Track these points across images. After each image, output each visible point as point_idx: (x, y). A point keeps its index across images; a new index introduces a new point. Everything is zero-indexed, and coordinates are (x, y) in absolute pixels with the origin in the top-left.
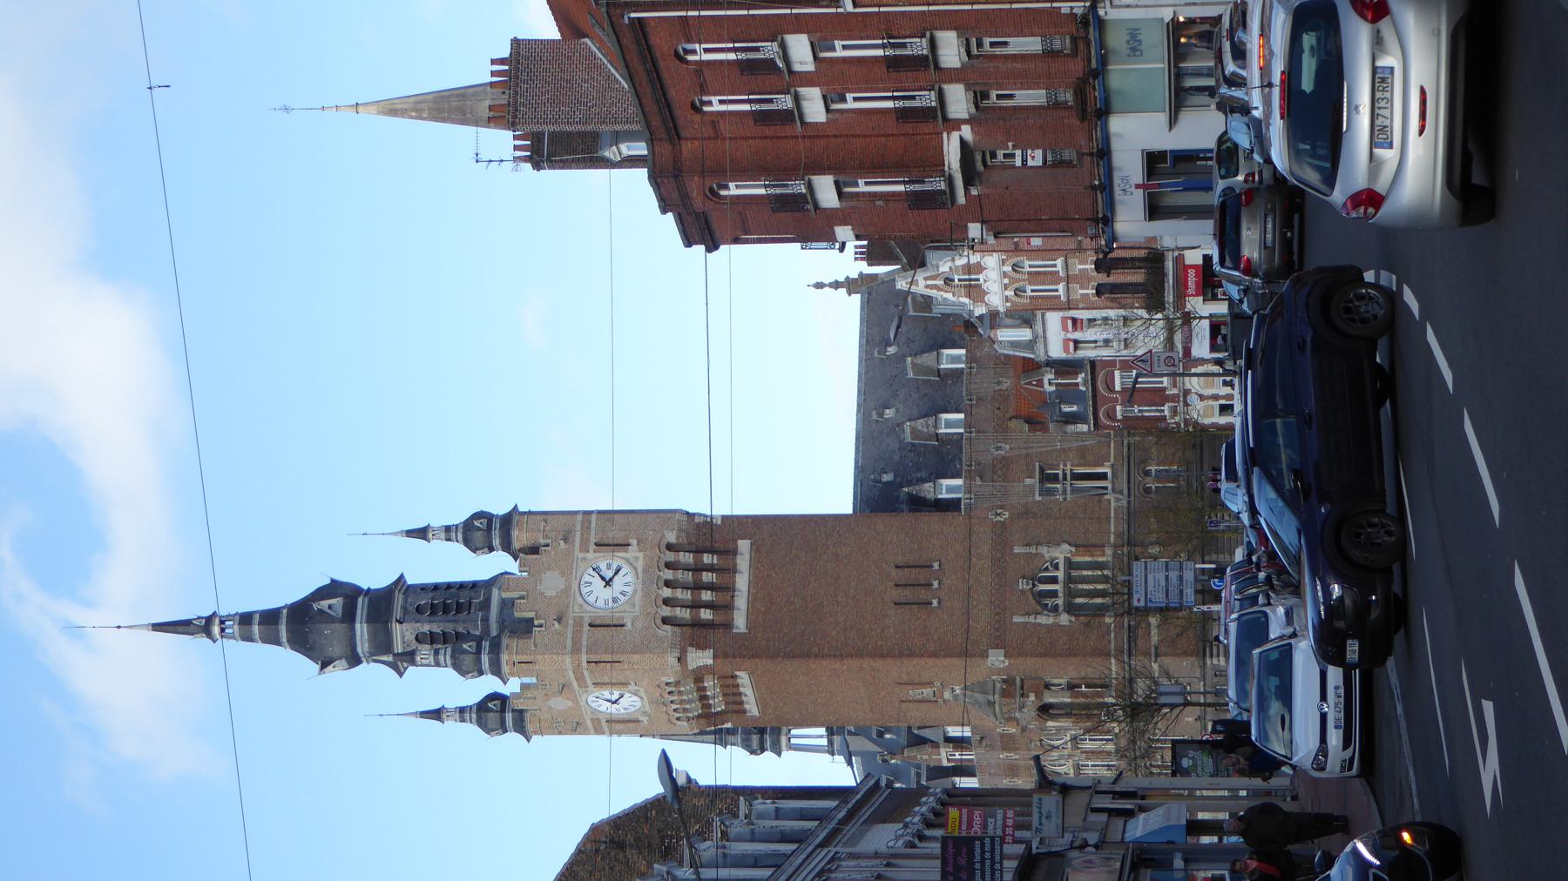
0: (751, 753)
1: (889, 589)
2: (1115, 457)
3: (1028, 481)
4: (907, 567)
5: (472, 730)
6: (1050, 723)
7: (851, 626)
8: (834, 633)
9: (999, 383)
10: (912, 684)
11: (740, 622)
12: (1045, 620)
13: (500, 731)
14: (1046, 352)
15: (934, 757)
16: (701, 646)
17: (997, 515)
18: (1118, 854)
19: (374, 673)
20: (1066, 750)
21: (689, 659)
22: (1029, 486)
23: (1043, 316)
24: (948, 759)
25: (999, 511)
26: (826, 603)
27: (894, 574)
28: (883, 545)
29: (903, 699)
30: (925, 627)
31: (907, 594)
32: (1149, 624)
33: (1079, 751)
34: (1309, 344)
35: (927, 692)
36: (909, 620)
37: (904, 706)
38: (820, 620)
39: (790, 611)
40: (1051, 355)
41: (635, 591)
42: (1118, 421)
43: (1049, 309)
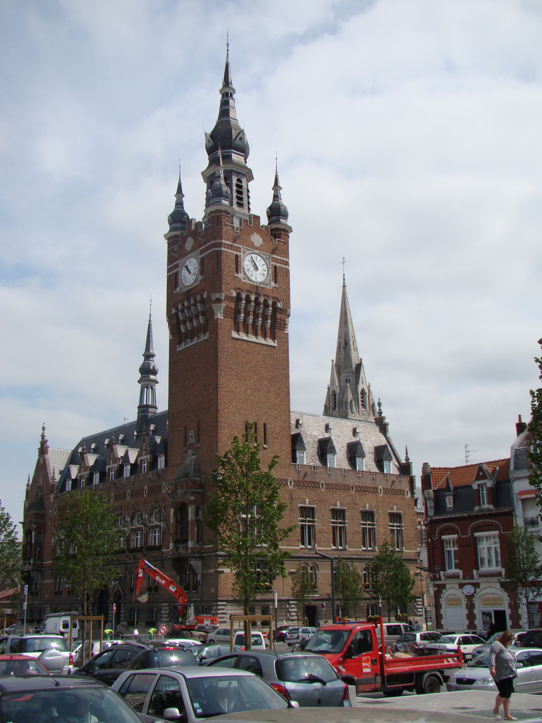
1: (254, 418)
3: (307, 501)
6: (172, 511)
7: (234, 395)
8: (231, 385)
13: (171, 221)
15: (144, 452)
17: (291, 482)
20: (148, 523)
22: (305, 501)
26: (246, 383)
27: (261, 422)
28: (275, 417)
33: (148, 530)
34: (86, 622)
38: (238, 379)
39: (242, 363)
42: (440, 537)
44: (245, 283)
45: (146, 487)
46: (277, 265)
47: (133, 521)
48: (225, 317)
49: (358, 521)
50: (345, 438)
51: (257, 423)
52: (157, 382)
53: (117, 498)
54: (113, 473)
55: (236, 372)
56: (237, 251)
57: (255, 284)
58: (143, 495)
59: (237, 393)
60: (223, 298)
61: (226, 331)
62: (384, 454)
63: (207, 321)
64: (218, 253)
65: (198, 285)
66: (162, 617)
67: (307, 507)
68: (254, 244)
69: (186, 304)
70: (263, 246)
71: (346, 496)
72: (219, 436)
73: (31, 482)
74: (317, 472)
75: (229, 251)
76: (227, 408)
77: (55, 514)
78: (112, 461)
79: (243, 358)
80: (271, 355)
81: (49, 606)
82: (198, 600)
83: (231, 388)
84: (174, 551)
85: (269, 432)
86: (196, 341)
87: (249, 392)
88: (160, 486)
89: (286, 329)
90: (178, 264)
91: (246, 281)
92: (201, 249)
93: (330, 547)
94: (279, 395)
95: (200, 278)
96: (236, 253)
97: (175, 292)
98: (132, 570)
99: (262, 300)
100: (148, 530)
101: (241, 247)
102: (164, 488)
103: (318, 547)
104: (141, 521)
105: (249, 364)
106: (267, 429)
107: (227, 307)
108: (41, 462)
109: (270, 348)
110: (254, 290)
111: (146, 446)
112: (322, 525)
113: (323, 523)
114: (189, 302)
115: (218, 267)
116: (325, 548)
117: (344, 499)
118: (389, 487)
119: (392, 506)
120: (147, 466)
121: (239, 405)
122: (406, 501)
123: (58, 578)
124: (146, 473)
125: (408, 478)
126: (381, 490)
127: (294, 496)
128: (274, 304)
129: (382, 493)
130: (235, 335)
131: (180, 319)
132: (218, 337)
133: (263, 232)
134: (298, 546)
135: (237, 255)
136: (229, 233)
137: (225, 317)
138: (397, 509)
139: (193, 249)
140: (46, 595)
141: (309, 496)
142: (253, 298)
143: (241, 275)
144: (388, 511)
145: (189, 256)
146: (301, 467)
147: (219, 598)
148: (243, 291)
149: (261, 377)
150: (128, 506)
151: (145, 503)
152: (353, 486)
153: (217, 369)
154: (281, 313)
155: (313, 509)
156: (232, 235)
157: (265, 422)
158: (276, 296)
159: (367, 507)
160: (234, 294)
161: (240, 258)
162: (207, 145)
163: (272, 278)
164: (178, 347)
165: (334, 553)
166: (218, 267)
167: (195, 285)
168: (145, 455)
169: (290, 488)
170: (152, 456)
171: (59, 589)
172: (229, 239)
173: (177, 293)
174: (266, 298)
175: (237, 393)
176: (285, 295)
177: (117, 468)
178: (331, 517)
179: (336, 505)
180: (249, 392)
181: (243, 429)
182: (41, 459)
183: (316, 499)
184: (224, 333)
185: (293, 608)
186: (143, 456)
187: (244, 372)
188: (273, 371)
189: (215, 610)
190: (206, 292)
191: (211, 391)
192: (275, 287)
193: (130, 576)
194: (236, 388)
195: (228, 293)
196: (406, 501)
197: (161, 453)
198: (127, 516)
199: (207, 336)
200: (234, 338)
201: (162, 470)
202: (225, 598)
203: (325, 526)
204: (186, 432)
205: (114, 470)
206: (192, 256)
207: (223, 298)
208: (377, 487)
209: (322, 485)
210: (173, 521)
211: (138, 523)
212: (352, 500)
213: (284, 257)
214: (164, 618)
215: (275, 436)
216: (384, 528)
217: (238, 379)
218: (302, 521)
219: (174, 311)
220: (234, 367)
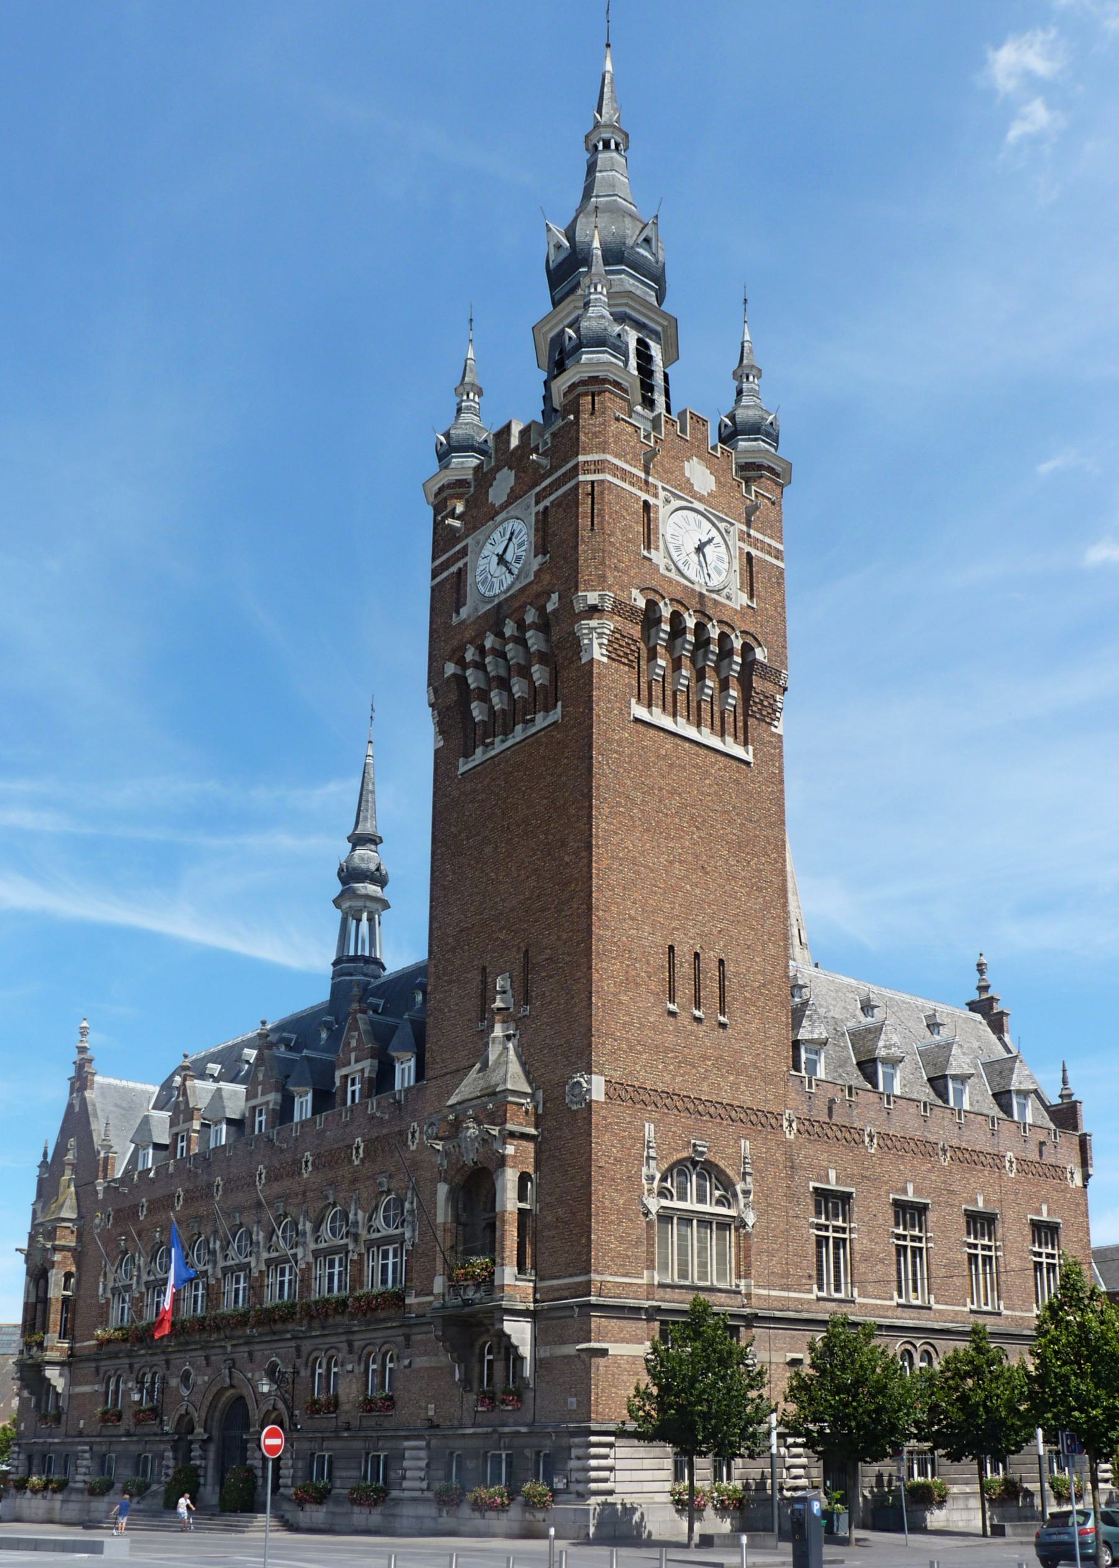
1: (691, 942)
2: (864, 1305)
6: (443, 1189)
15: (353, 1055)
18: (747, 407)
22: (827, 1175)
24: (346, 1076)
30: (637, 985)
31: (685, 969)
36: (648, 962)
37: (475, 976)
39: (661, 789)
44: (670, 581)
45: (359, 1139)
46: (754, 552)
47: (318, 1231)
48: (613, 659)
49: (957, 1236)
50: (909, 1034)
51: (701, 956)
52: (386, 905)
53: (274, 1176)
54: (263, 1118)
55: (642, 811)
56: (647, 492)
57: (697, 588)
58: (351, 1162)
59: (646, 867)
60: (608, 605)
61: (616, 696)
62: (1015, 1076)
64: (593, 487)
65: (531, 583)
66: (404, 1478)
67: (832, 1191)
68: (692, 485)
69: (489, 642)
70: (715, 497)
71: (929, 1171)
72: (595, 976)
73: (49, 1159)
74: (857, 1104)
76: (616, 903)
77: (109, 1227)
78: (260, 1088)
79: (663, 777)
80: (737, 782)
81: (87, 1448)
82: (524, 1430)
83: (630, 851)
84: (447, 1298)
85: (731, 984)
86: (519, 733)
87: (678, 869)
88: (402, 1133)
89: (776, 723)
90: (465, 548)
91: (673, 575)
92: (538, 489)
93: (891, 1299)
94: (760, 889)
95: (536, 563)
96: (645, 496)
97: (455, 620)
98: (315, 1354)
99: (714, 633)
100: (363, 1251)
101: (660, 484)
102: (413, 1136)
103: (859, 1296)
104: (344, 1230)
105: (680, 794)
106: (728, 974)
107: (618, 631)
108: (77, 1109)
109: (735, 764)
110: (694, 603)
111: (359, 1040)
112: (872, 1240)
113: (873, 1235)
114: (500, 634)
116: (879, 1302)
117: (924, 1178)
118: (1034, 1156)
119: (1038, 1205)
120: (361, 1090)
121: (651, 902)
122: (1069, 1196)
123: (113, 1380)
124: (360, 1104)
125: (1076, 1141)
126: (1011, 1162)
127: (799, 1159)
128: (747, 649)
129: (1015, 1171)
130: (640, 711)
131: (468, 686)
132: (591, 709)
133: (716, 461)
134: (810, 1291)
135: (646, 503)
136: (626, 440)
137: (613, 659)
138: (1049, 1214)
139: (514, 497)
140: (82, 1422)
141: (836, 1162)
142: (691, 622)
143: (657, 557)
144: (1029, 1217)
145: (498, 518)
146: (817, 1085)
147: (594, 1426)
148: (663, 598)
149: (711, 835)
150: (304, 1193)
151: (354, 1181)
152: (947, 1147)
153: (590, 797)
154: (764, 677)
155: (849, 1195)
156: (633, 447)
157: (722, 956)
158: (752, 630)
159: (981, 1204)
160: (641, 603)
161: (657, 512)
162: (552, 258)
163: (742, 583)
164: (460, 764)
165: (899, 1315)
167: (518, 586)
168: (357, 1061)
169: (788, 1136)
170: (376, 1062)
171: (116, 1405)
172: (624, 456)
173: (463, 622)
174: (727, 630)
175: (646, 867)
176: (774, 633)
177: (276, 1103)
178: (892, 1222)
179: (904, 1191)
180: (678, 869)
181: (663, 967)
182: (76, 1102)
183: (855, 1172)
184: (609, 702)
185: (798, 1456)
186: (349, 1064)
187: (666, 815)
188: (742, 824)
189: (578, 1458)
190: (555, 597)
191: (567, 859)
192: (749, 606)
193: (309, 1369)
194: (642, 853)
195: (622, 596)
196: (1069, 1196)
197: (405, 1049)
198: (301, 1219)
199: (556, 715)
200: (637, 720)
201: (408, 1090)
202: (612, 1427)
203: (877, 1243)
204: (484, 982)
205: (267, 1109)
206: (512, 513)
207: (608, 605)
208: (1004, 1154)
209: (871, 1137)
210: (446, 1215)
211: (335, 1236)
212: (945, 1182)
213: (772, 537)
214: (413, 1479)
215: (747, 995)
216: (1021, 1258)
217: (648, 830)
218: (819, 1227)
219: (450, 669)
220: (638, 796)
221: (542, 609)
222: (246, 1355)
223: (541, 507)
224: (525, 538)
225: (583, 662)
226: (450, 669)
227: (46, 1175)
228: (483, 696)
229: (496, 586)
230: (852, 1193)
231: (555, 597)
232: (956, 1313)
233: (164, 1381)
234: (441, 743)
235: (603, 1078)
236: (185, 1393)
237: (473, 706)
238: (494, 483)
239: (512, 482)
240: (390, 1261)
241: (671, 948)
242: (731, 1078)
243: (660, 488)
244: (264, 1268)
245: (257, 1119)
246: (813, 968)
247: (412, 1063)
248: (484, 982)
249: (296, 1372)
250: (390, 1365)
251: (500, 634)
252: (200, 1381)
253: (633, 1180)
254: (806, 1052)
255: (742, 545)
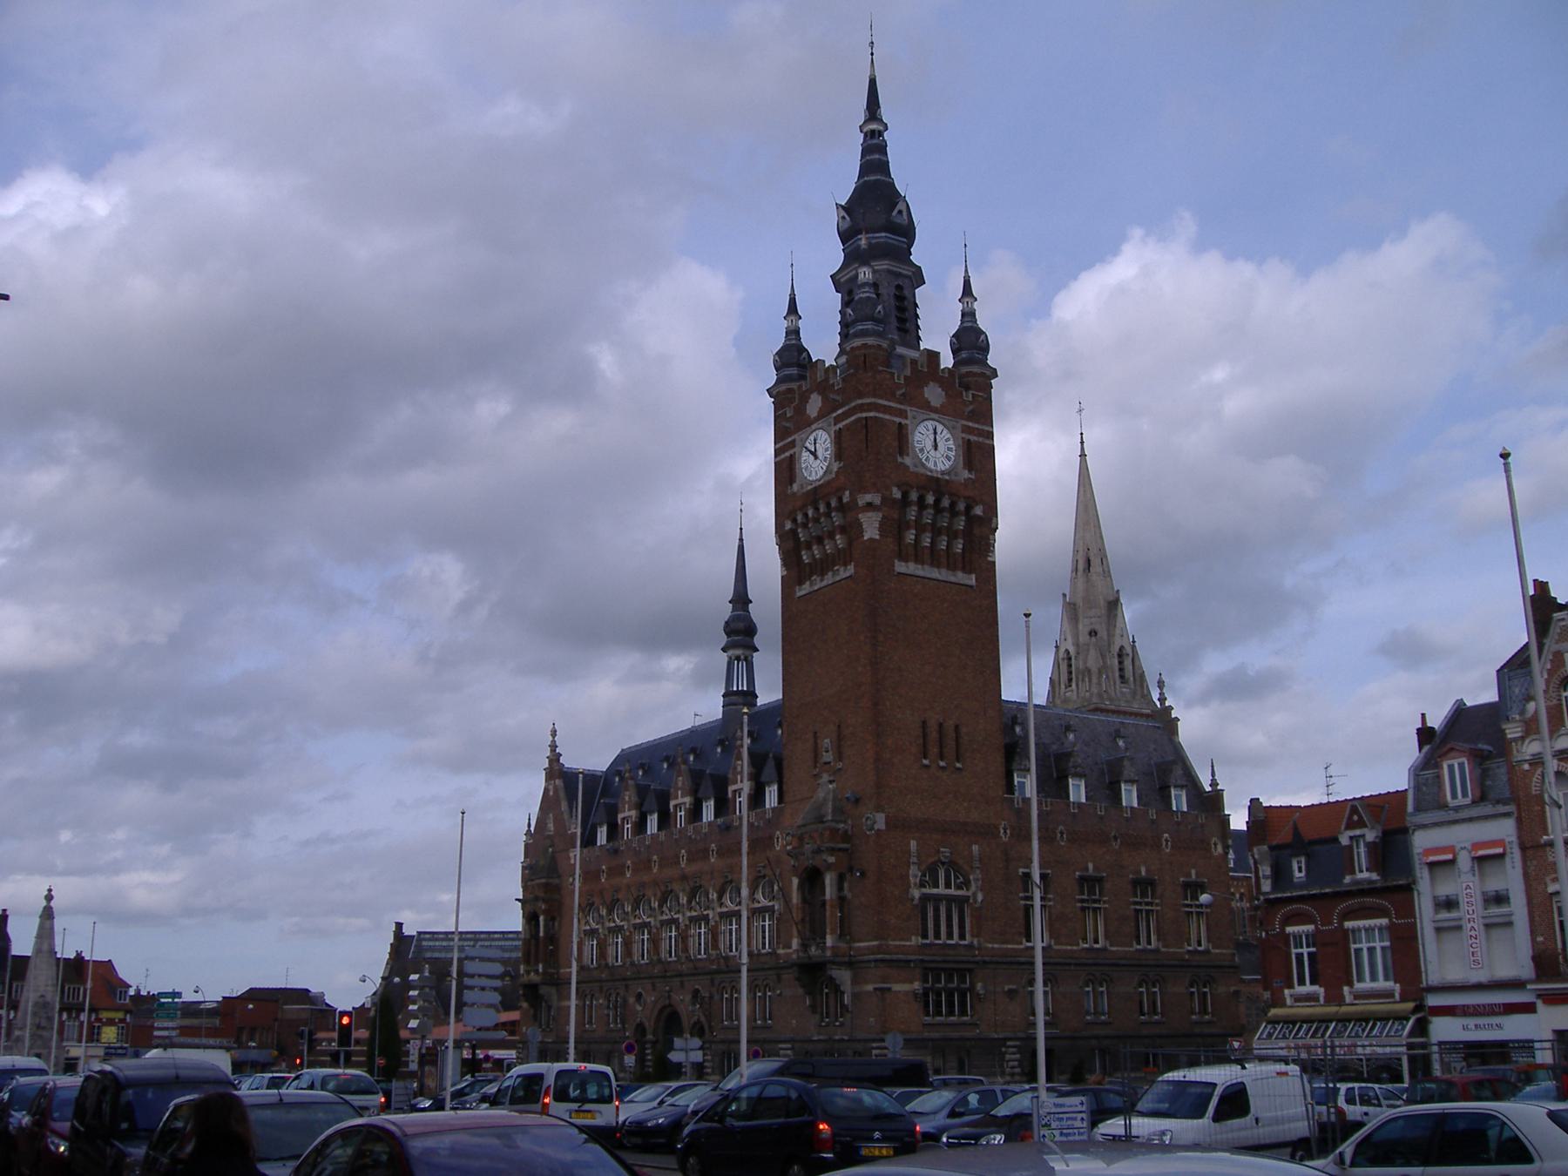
0: (726, 623)
2: (1059, 950)
4: (957, 737)
5: (779, 342)
6: (795, 881)
9: (1115, 838)
10: (840, 738)
11: (900, 567)
12: (914, 873)
14: (1424, 826)
16: (882, 528)
19: (833, 255)
21: (870, 514)
23: (1507, 815)
24: (735, 791)
25: (1008, 832)
27: (951, 722)
29: (818, 734)
32: (912, 982)
35: (828, 757)
40: (1417, 833)
41: (931, 471)
43: (1519, 821)
63: (850, 544)
73: (532, 829)
75: (887, 417)
88: (771, 838)
90: (794, 441)
96: (897, 420)
115: (867, 447)
131: (799, 539)
145: (813, 427)
150: (712, 873)
164: (797, 590)
166: (867, 447)
190: (847, 493)
201: (774, 809)
204: (816, 743)
219: (788, 525)
221: (840, 499)
222: (678, 983)
223: (837, 427)
224: (829, 445)
225: (865, 538)
226: (788, 525)
227: (531, 841)
228: (809, 547)
229: (814, 474)
230: (1049, 874)
231: (847, 493)
232: (1127, 952)
233: (625, 1001)
234: (785, 573)
235: (883, 815)
236: (639, 1008)
237: (803, 553)
238: (810, 401)
239: (820, 404)
240: (767, 923)
241: (924, 723)
242: (965, 804)
243: (909, 411)
244: (688, 923)
245: (679, 814)
246: (1087, 630)
247: (776, 787)
248: (816, 743)
249: (711, 997)
250: (769, 994)
251: (817, 509)
252: (648, 1001)
253: (905, 878)
254: (1018, 777)
255: (964, 435)
